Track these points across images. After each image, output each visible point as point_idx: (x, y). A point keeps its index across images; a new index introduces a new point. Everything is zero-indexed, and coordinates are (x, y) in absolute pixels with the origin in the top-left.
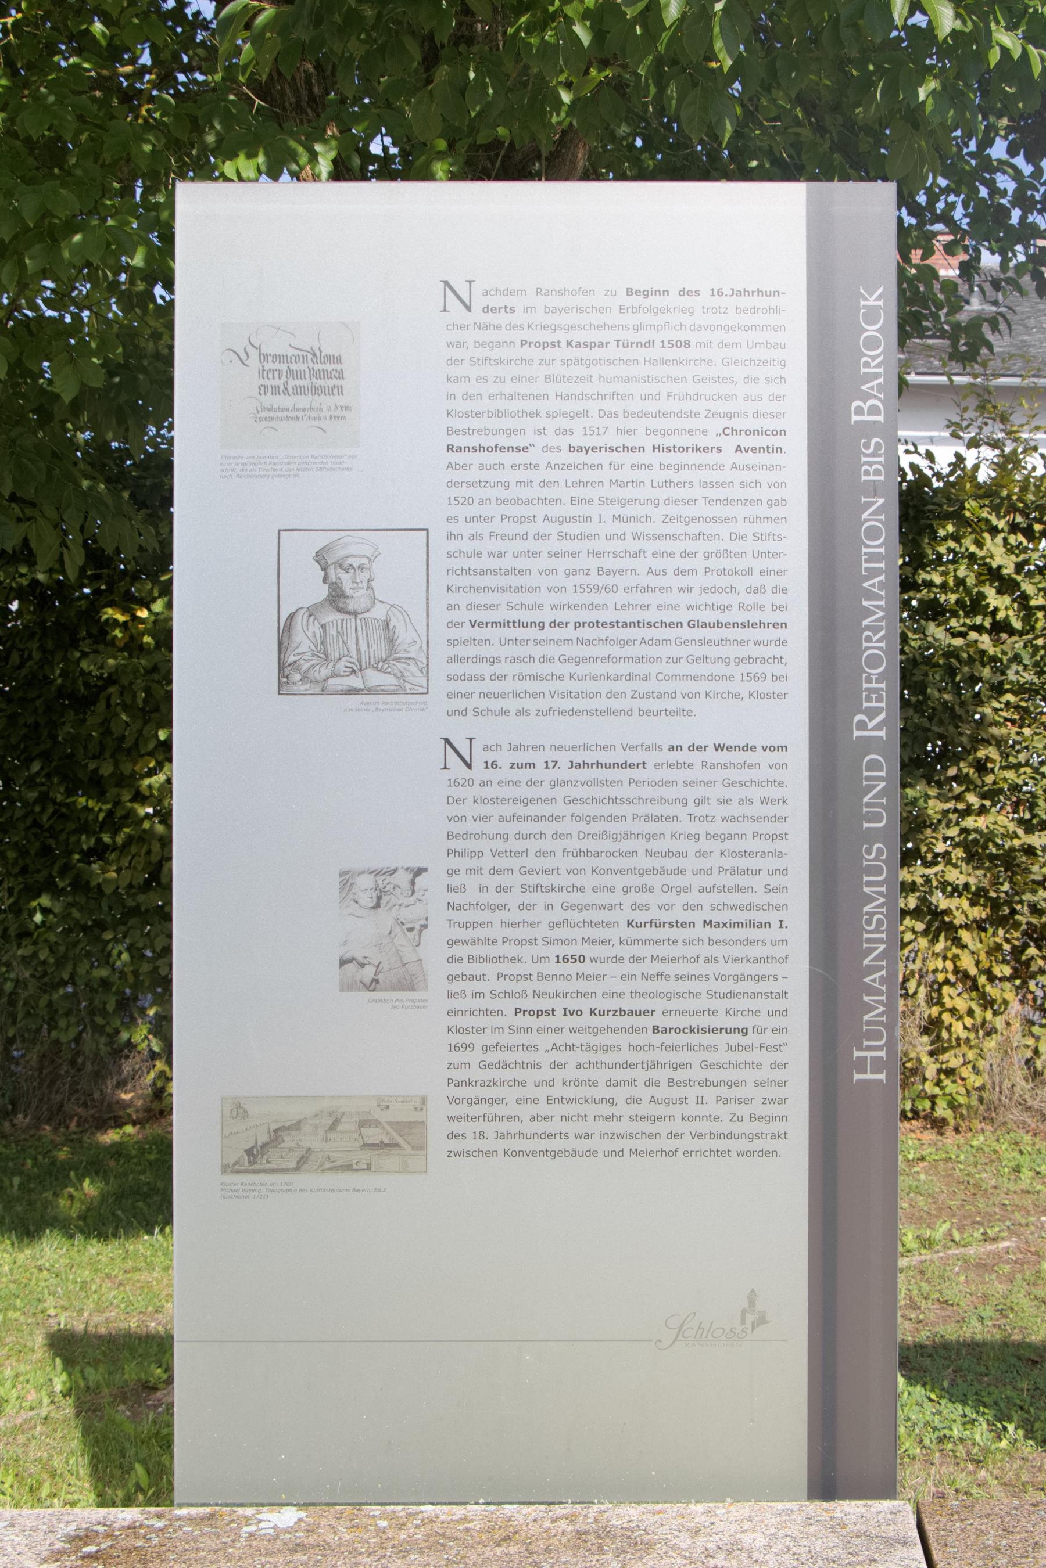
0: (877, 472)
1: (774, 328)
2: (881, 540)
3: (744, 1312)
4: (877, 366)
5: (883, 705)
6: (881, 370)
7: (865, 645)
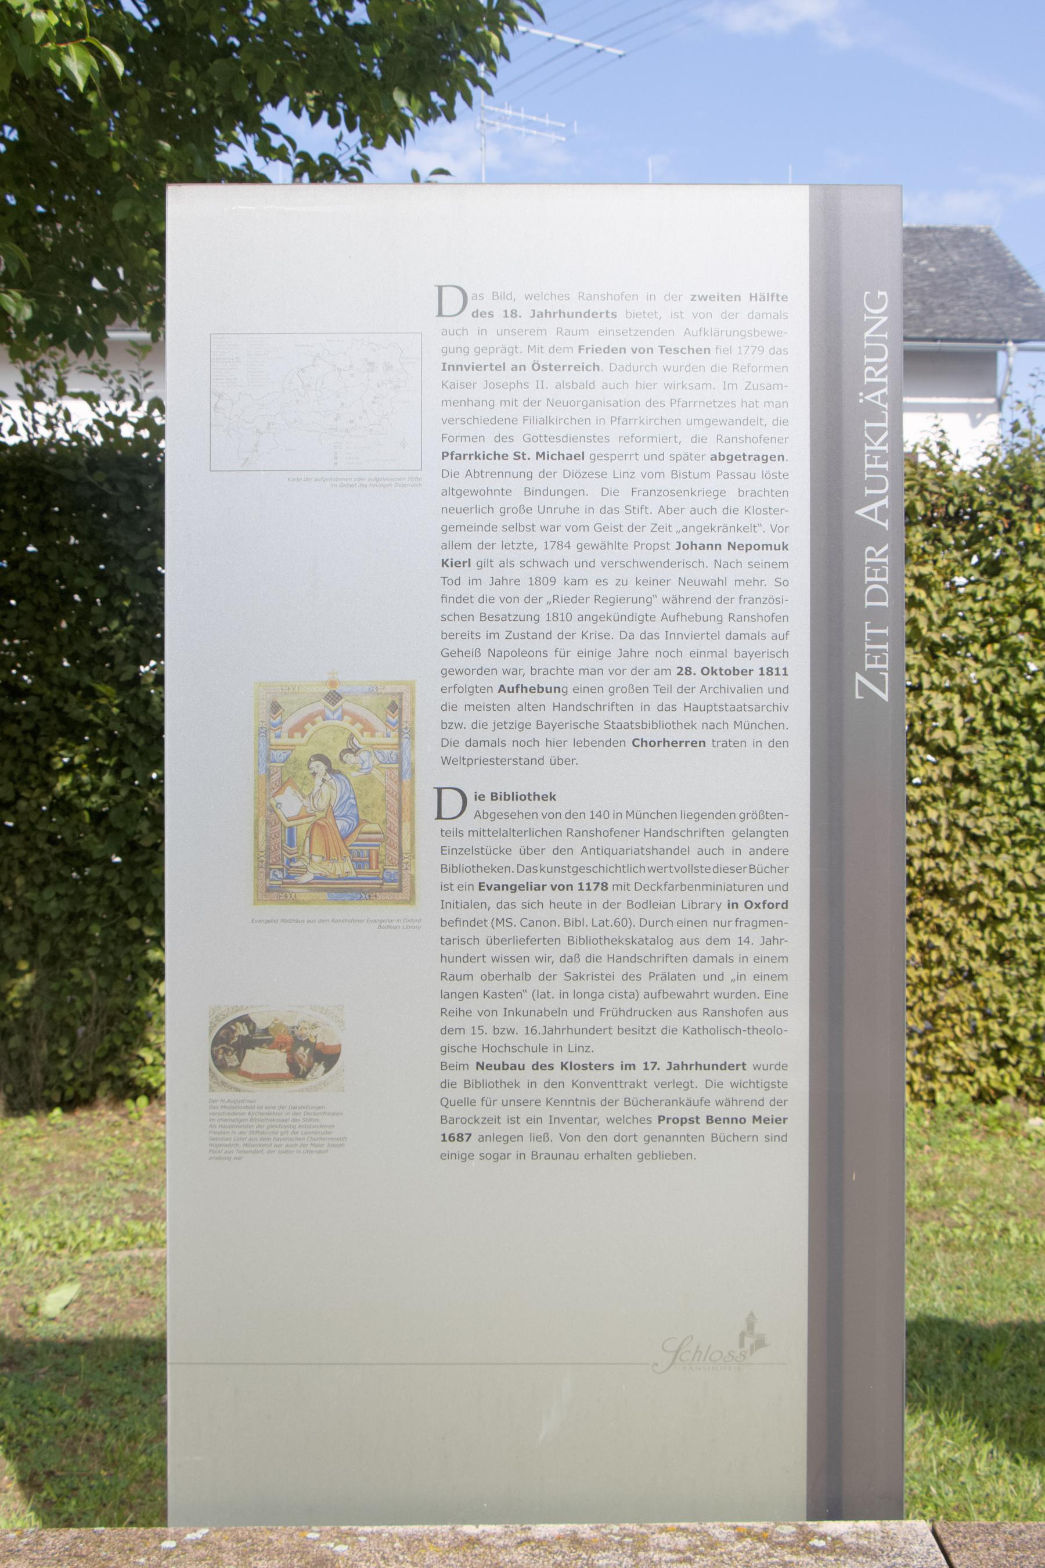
3: (742, 1335)
4: (882, 375)
5: (886, 666)
7: (867, 579)
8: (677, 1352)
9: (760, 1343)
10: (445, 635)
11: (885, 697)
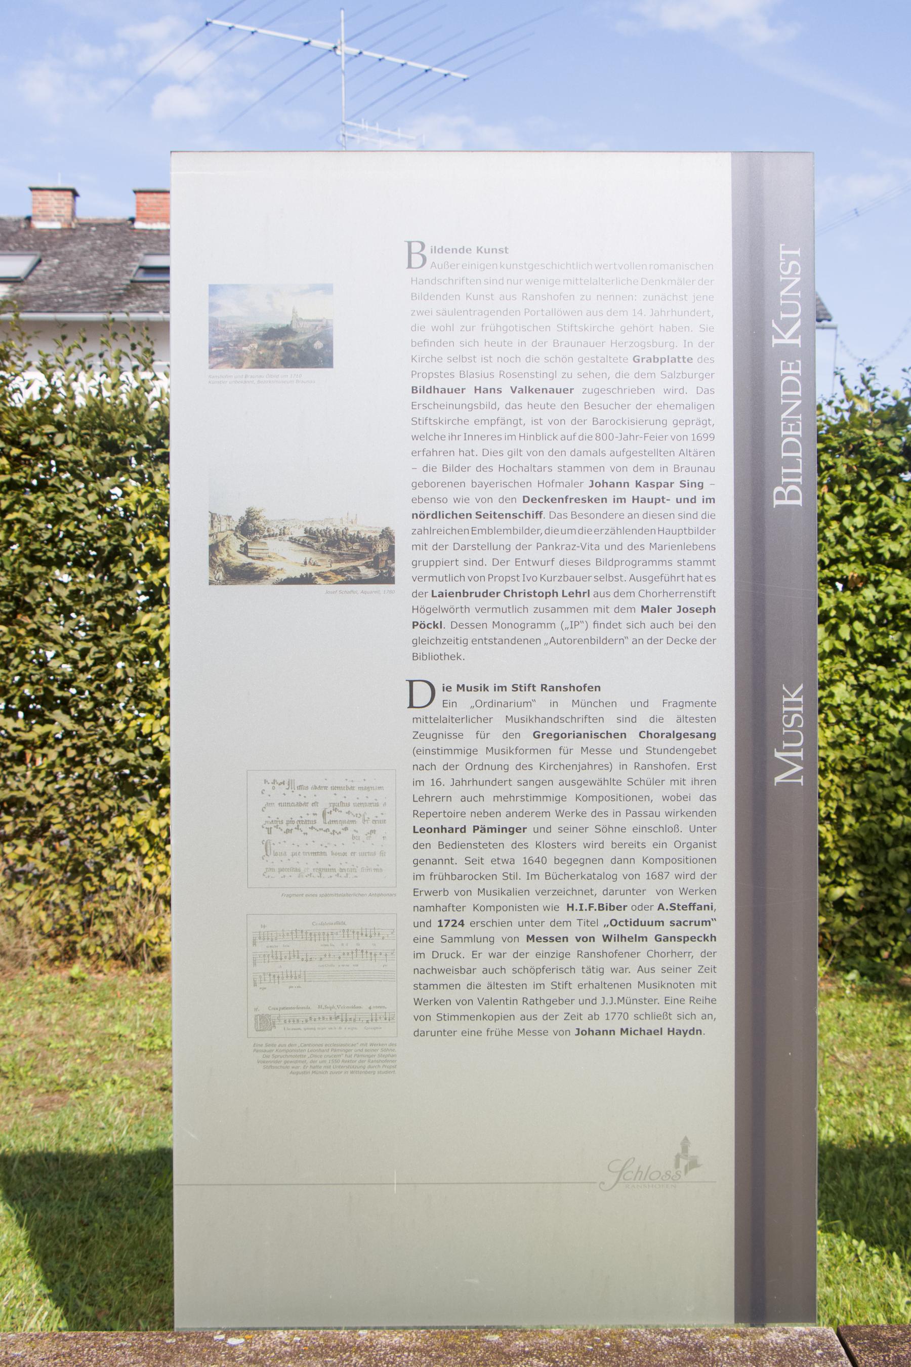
0: (793, 495)
3: (678, 1157)
6: (801, 699)
7: (783, 433)
9: (694, 1164)
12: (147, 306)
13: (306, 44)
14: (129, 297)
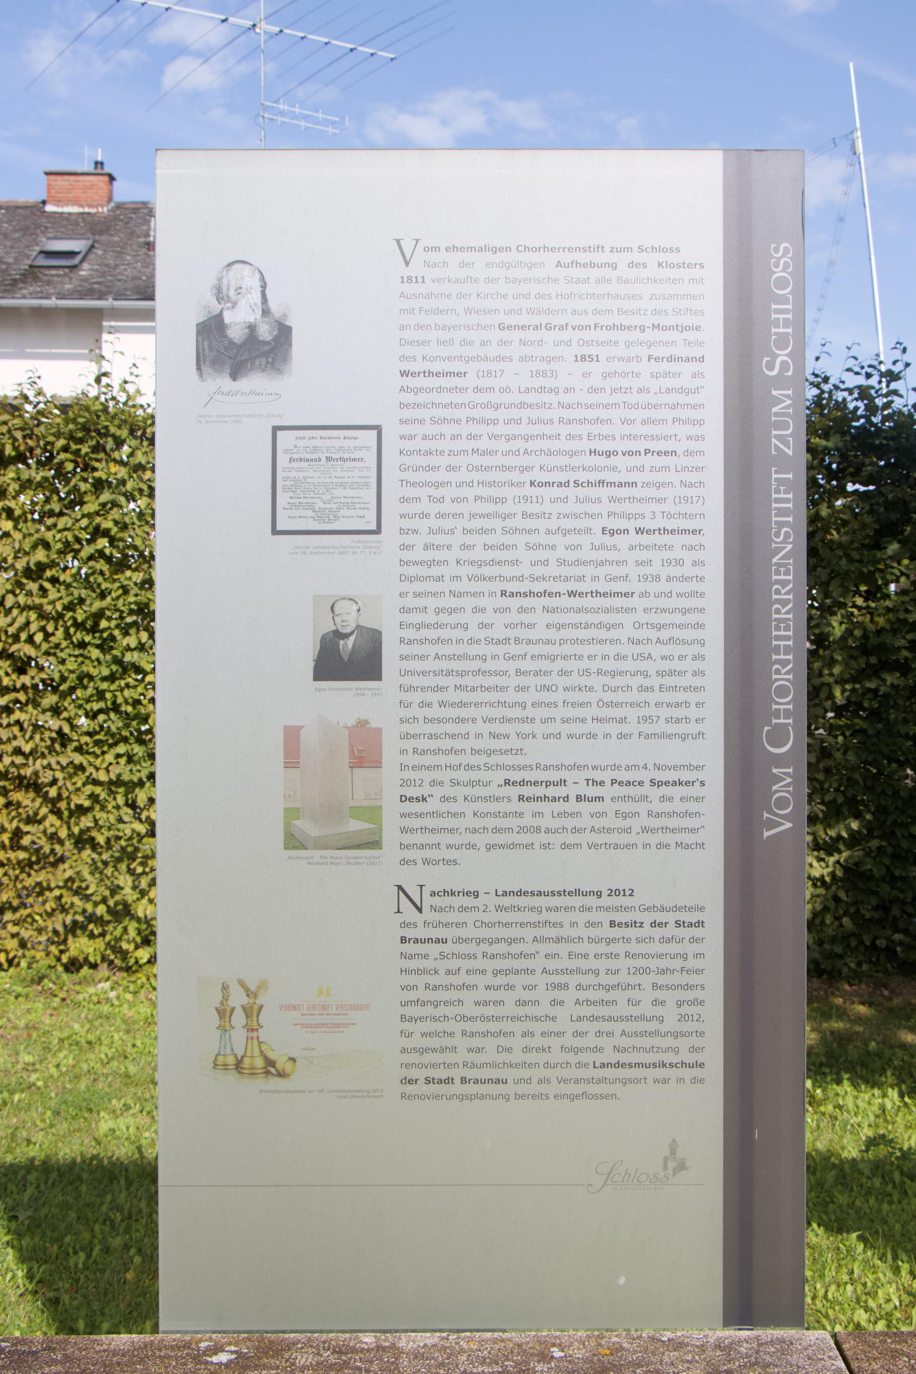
1: (694, 407)
2: (789, 810)
3: (666, 1159)
5: (790, 577)
6: (790, 597)
7: (774, 677)
8: (609, 1174)
10: (403, 406)
11: (790, 453)
12: (41, 292)
13: (223, 21)
14: (24, 282)
